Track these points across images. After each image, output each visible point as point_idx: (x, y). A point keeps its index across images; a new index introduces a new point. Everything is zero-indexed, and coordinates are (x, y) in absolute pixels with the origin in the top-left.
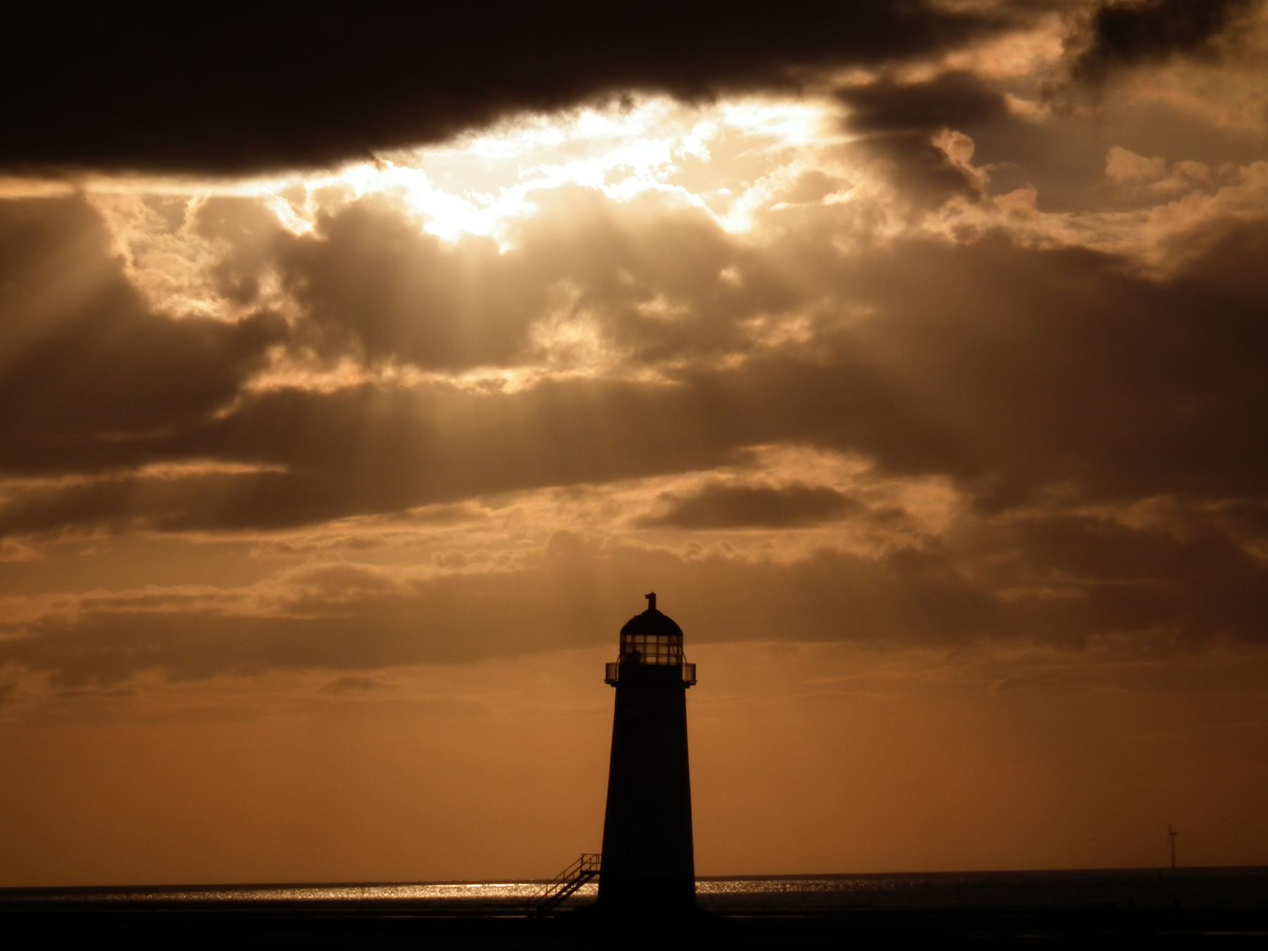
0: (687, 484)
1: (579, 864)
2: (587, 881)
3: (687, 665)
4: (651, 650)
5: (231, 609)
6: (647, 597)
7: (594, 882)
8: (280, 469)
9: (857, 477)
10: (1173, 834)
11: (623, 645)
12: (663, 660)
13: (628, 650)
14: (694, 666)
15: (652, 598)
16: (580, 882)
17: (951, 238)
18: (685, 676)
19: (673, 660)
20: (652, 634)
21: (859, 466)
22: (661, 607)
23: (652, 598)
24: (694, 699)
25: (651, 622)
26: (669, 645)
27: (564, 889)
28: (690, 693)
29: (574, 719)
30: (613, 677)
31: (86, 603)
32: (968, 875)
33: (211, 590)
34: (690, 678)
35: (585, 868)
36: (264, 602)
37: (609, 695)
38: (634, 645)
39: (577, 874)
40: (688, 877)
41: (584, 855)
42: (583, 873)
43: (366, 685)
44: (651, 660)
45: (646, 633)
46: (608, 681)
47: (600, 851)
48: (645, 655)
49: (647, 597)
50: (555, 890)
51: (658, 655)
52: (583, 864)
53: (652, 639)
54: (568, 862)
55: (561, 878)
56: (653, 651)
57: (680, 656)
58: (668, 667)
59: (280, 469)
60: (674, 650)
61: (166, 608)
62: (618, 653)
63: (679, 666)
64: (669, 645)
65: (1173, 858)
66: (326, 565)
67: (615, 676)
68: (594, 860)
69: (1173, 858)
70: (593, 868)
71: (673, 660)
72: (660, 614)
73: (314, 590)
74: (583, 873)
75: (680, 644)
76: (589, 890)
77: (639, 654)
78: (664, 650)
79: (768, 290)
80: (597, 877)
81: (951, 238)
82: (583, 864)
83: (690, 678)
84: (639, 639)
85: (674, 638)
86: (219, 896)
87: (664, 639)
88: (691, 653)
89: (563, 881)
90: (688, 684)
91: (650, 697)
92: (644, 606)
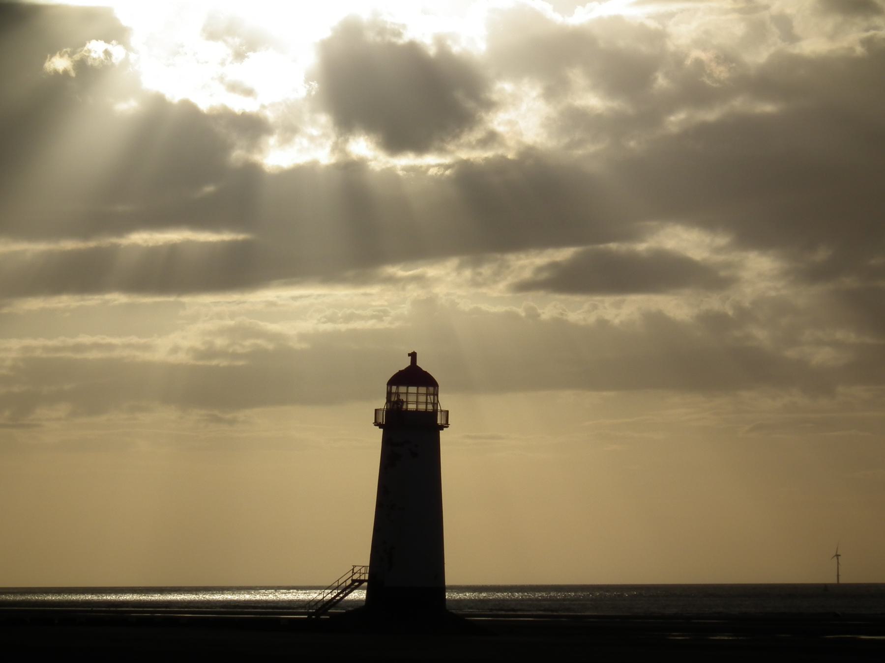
0: (564, 254)
1: (350, 574)
2: (356, 588)
3: (441, 411)
4: (412, 398)
5: (148, 356)
6: (409, 355)
7: (363, 589)
8: (241, 237)
9: (718, 250)
10: (837, 556)
11: (389, 394)
12: (422, 407)
13: (394, 398)
14: (447, 412)
15: (413, 356)
16: (351, 588)
17: (860, 50)
18: (440, 420)
19: (430, 407)
20: (422, 385)
21: (722, 240)
22: (419, 363)
23: (413, 356)
24: (448, 441)
25: (413, 376)
26: (427, 394)
27: (338, 595)
28: (444, 435)
29: (350, 457)
30: (380, 421)
31: (26, 349)
32: (761, 585)
33: (134, 340)
34: (443, 422)
35: (355, 577)
36: (175, 349)
37: (378, 434)
38: (398, 394)
39: (349, 582)
40: (441, 588)
41: (354, 566)
42: (354, 581)
43: (232, 422)
44: (412, 407)
45: (409, 384)
46: (377, 423)
47: (368, 564)
48: (407, 402)
49: (409, 355)
50: (328, 595)
51: (417, 403)
52: (354, 574)
53: (413, 389)
54: (340, 573)
55: (336, 584)
56: (414, 399)
57: (435, 404)
58: (426, 412)
59: (226, 236)
60: (431, 398)
61: (93, 355)
62: (385, 401)
63: (435, 413)
64: (427, 394)
65: (838, 575)
66: (231, 323)
67: (382, 419)
68: (363, 571)
69: (838, 575)
70: (362, 578)
71: (430, 407)
72: (420, 369)
73: (220, 342)
74: (354, 581)
75: (436, 394)
76: (359, 595)
77: (402, 402)
78: (422, 399)
79: (694, 89)
80: (365, 584)
81: (860, 50)
82: (354, 574)
83: (443, 422)
84: (403, 389)
85: (431, 389)
86: (50, 597)
87: (423, 390)
88: (445, 401)
89: (337, 588)
90: (442, 427)
91: (410, 442)
92: (406, 363)
